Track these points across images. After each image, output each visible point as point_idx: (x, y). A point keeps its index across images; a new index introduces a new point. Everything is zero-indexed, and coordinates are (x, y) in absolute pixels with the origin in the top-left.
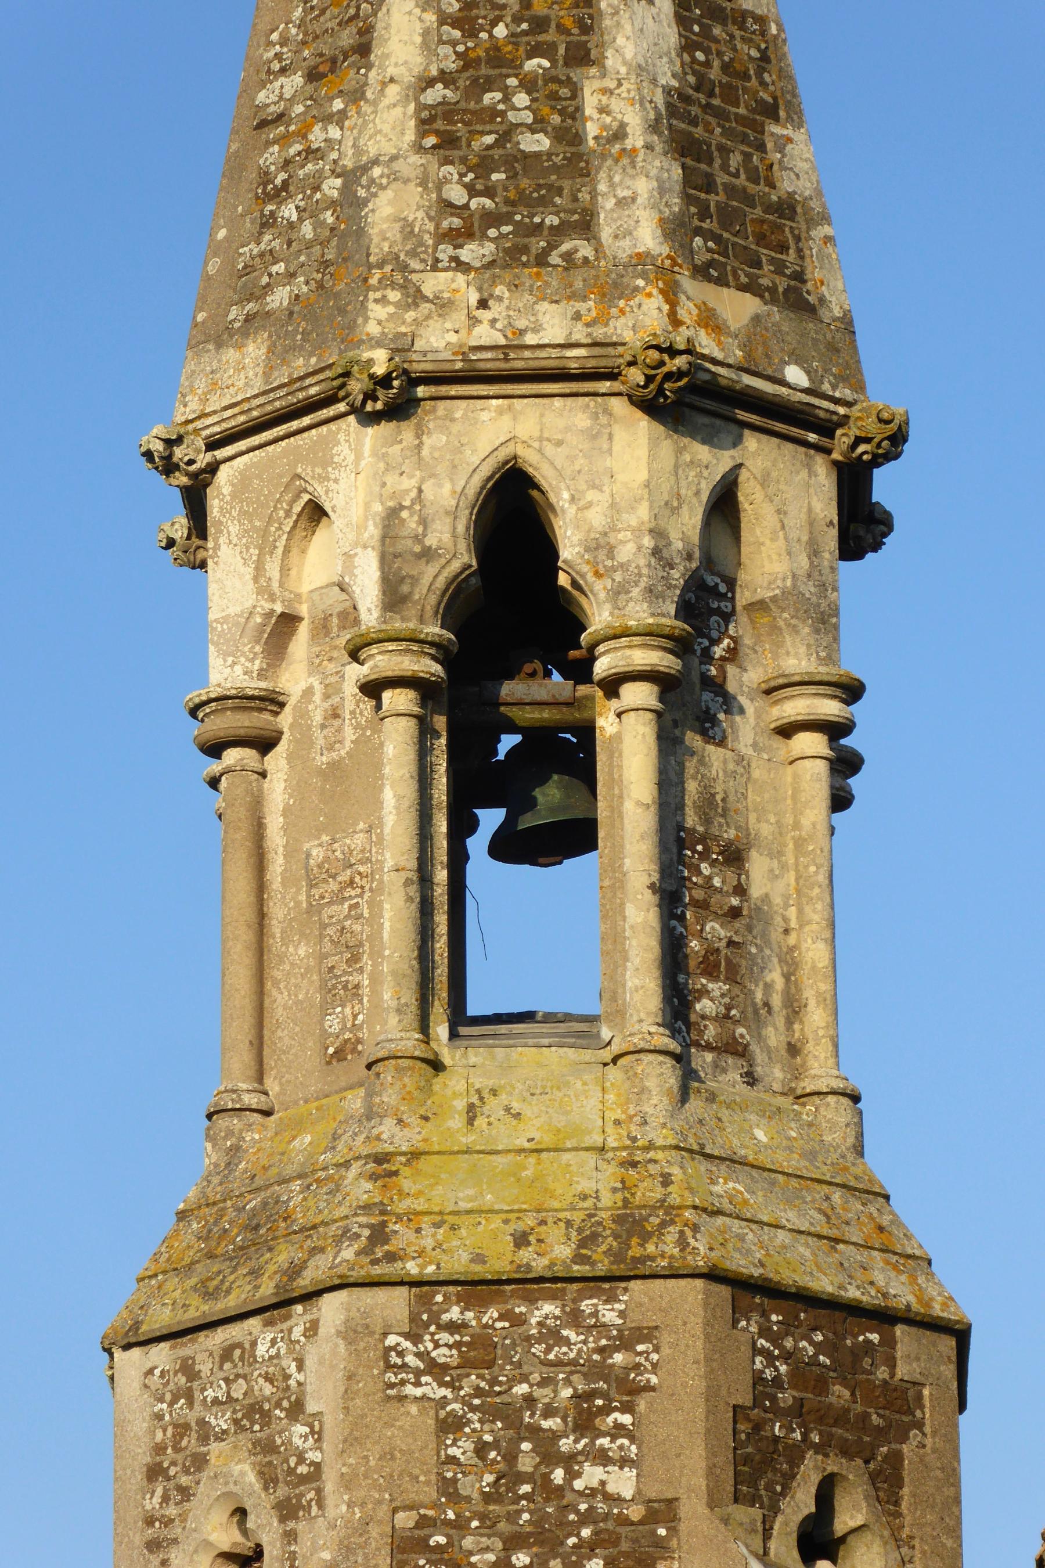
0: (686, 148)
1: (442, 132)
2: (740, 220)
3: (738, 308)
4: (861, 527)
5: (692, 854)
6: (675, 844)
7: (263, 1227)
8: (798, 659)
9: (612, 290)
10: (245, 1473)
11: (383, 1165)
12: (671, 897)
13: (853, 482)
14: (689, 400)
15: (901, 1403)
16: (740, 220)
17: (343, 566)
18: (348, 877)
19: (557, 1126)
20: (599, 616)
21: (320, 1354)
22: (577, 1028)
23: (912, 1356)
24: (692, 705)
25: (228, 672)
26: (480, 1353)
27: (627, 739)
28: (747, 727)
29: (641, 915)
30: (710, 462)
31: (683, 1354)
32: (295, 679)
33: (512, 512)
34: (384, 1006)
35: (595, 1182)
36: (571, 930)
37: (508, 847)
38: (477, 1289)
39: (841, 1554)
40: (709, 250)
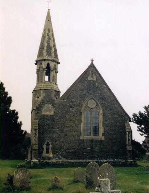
9: (52, 57)
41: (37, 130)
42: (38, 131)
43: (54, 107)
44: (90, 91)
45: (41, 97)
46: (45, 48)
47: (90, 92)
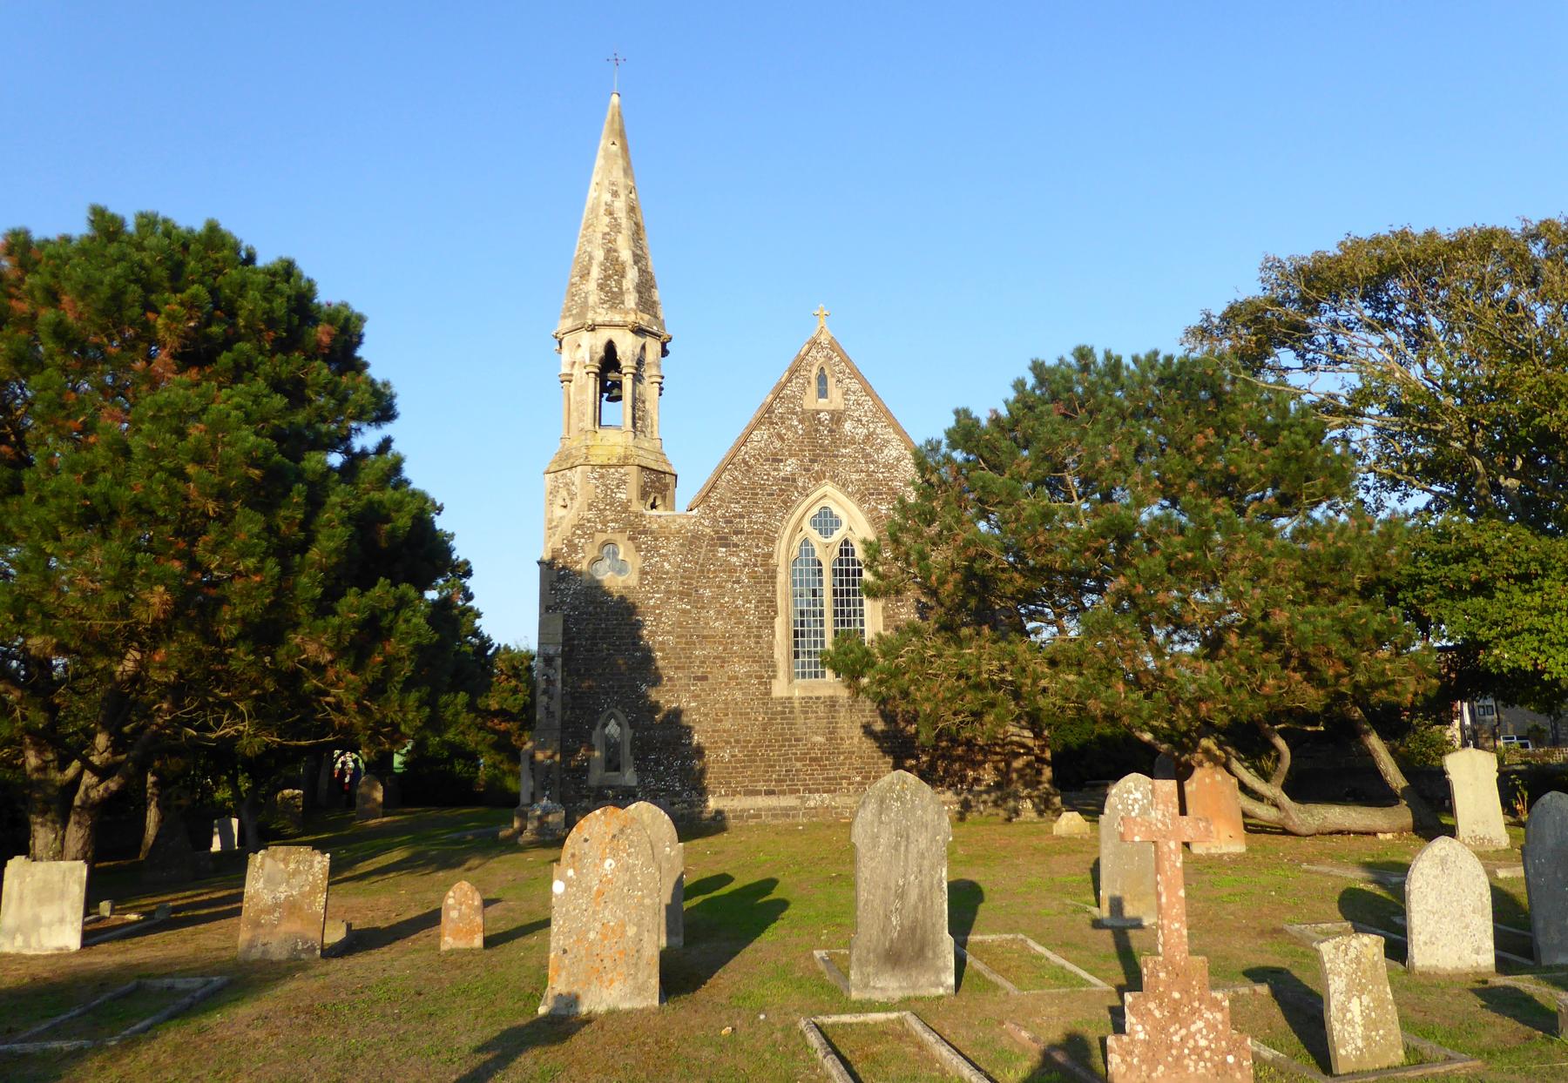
0: (639, 292)
1: (601, 287)
2: (647, 303)
3: (647, 317)
4: (665, 353)
5: (637, 401)
6: (635, 400)
7: (569, 456)
8: (654, 372)
9: (627, 313)
10: (565, 493)
11: (587, 447)
12: (634, 408)
13: (664, 345)
14: (639, 331)
15: (667, 486)
16: (647, 303)
17: (583, 354)
18: (582, 402)
19: (615, 441)
20: (623, 364)
21: (576, 475)
22: (619, 428)
23: (668, 479)
24: (637, 378)
25: (565, 370)
26: (602, 476)
27: (627, 382)
28: (646, 382)
29: (629, 410)
30: (641, 341)
31: (633, 477)
32: (576, 371)
33: (610, 348)
34: (588, 423)
35: (621, 451)
36: (617, 413)
37: (609, 399)
38: (602, 466)
39: (671, 999)
40: (901, 988)
41: (559, 661)
42: (563, 665)
43: (638, 549)
44: (813, 461)
45: (576, 504)
46: (596, 272)
47: (816, 467)
